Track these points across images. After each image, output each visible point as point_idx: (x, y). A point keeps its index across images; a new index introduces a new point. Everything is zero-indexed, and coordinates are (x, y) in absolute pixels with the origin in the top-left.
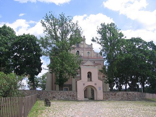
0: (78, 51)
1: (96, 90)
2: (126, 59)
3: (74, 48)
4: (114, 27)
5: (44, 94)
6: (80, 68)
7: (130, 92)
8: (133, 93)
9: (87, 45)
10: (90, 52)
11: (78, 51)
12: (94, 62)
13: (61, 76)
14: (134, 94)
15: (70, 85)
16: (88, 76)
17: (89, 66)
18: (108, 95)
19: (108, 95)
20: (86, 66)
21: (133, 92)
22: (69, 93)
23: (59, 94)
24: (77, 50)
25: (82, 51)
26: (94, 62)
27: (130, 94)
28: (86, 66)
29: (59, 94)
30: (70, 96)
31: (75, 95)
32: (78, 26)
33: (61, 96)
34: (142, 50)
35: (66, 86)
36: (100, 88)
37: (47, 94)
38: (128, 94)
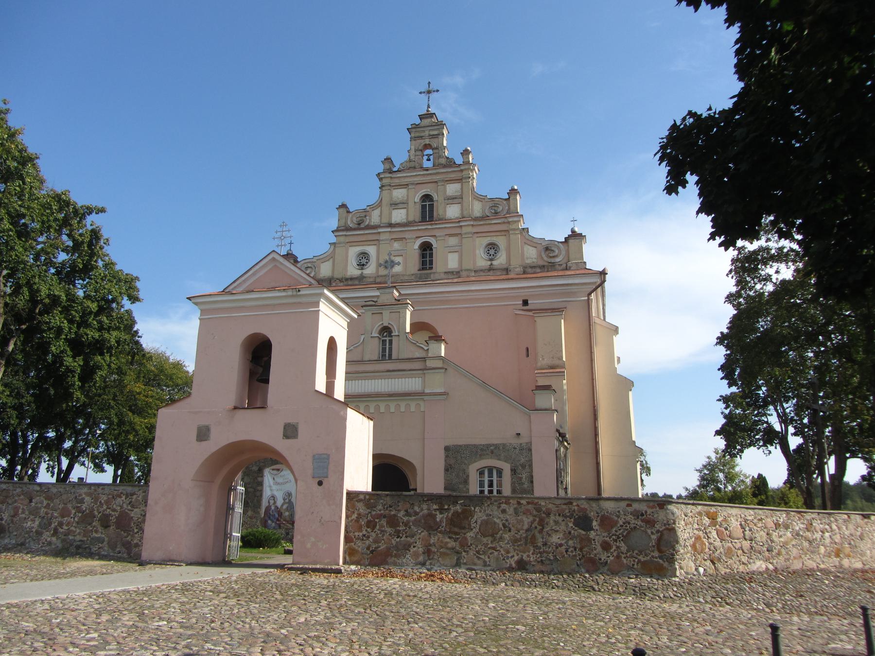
10: (501, 241)
11: (426, 248)
12: (525, 303)
19: (393, 522)
24: (418, 242)
25: (453, 241)
26: (525, 303)
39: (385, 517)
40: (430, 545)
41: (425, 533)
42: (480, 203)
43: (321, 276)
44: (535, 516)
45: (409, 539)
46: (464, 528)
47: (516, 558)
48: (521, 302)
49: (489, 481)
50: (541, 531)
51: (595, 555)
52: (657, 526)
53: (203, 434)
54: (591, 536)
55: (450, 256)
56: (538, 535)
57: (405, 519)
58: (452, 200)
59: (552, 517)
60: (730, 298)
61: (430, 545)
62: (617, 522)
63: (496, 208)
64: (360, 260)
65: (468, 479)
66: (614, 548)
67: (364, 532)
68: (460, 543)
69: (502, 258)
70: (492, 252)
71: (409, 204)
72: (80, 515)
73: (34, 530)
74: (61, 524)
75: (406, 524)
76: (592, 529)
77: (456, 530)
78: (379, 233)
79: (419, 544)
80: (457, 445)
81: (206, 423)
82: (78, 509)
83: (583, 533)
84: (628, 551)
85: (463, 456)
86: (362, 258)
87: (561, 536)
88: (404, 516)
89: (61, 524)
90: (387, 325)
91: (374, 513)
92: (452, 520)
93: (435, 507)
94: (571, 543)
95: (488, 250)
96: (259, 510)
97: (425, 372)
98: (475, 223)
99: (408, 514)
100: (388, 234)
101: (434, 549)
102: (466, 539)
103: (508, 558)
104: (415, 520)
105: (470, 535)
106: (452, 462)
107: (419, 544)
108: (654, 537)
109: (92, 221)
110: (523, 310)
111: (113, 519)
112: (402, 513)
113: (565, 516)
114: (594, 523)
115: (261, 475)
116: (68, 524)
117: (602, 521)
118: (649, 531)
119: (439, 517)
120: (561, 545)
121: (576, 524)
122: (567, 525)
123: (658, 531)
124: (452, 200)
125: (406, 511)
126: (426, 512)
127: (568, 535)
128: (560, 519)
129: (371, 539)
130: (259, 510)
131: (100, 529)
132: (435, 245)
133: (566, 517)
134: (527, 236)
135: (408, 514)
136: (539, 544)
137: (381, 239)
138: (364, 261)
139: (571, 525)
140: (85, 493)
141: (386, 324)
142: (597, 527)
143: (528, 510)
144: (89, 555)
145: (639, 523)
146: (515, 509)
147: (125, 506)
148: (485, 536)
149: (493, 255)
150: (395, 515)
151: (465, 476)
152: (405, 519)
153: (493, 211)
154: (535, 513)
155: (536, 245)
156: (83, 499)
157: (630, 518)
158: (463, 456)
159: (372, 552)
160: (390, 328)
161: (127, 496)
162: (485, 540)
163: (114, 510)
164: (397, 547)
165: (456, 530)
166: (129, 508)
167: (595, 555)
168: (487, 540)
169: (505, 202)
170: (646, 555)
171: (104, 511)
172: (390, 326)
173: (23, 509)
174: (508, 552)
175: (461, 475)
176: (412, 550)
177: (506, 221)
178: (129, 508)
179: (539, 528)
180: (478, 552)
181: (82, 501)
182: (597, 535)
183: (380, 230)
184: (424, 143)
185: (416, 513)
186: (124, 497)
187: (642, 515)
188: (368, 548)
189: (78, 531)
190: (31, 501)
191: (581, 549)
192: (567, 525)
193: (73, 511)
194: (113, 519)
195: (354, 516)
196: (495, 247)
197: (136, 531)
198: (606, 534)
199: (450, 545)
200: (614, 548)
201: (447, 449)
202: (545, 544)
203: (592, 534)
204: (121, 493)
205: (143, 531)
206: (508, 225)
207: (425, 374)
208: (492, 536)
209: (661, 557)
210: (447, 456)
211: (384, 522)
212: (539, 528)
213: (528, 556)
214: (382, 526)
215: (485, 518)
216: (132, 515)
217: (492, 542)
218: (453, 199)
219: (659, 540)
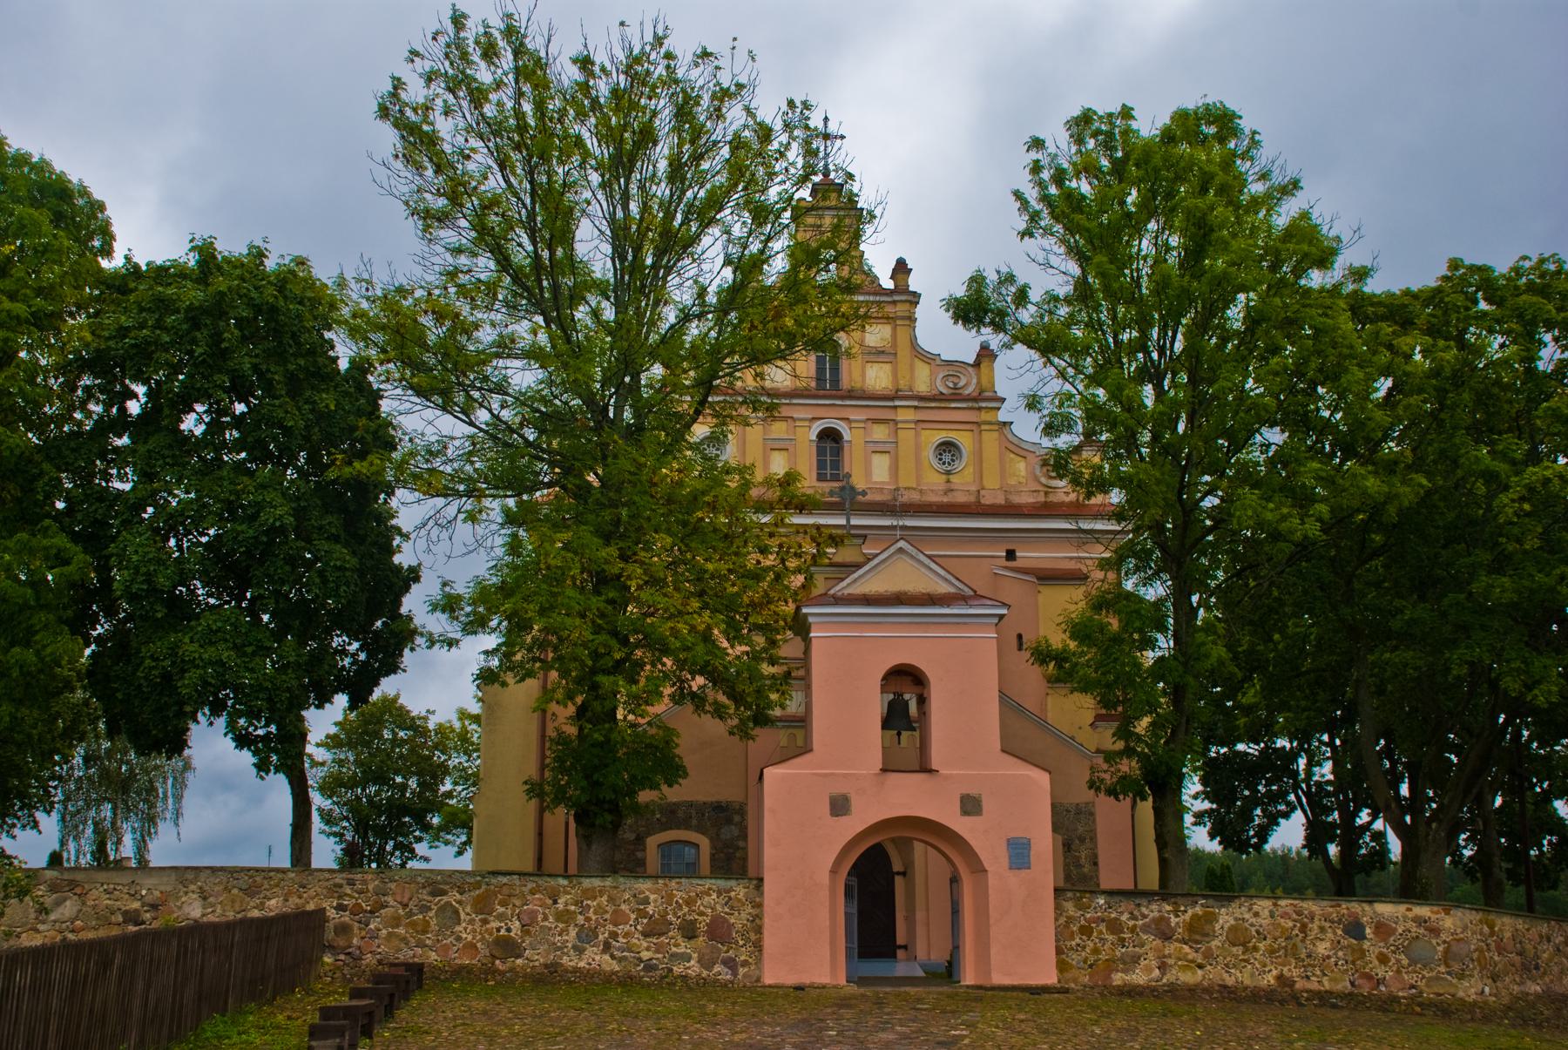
0: (830, 437)
1: (978, 869)
2: (1338, 523)
3: (768, 404)
4: (1234, 154)
5: (393, 908)
6: (801, 627)
7: (1385, 909)
8: (1420, 921)
9: (929, 358)
10: (964, 440)
11: (830, 437)
12: (1011, 555)
13: (595, 713)
14: (1435, 931)
15: (719, 808)
16: (896, 718)
17: (899, 599)
18: (1115, 927)
19: (1115, 927)
20: (867, 600)
21: (1423, 911)
22: (669, 898)
23: (560, 916)
24: (817, 427)
25: (880, 433)
26: (1011, 555)
27: (1383, 929)
28: (867, 600)
29: (560, 916)
30: (689, 932)
31: (739, 920)
32: (1052, 149)
33: (587, 936)
34: (96, 570)
35: (673, 816)
36: (1019, 853)
37: (425, 909)
38: (1355, 929)
39: (1103, 921)
40: (1165, 957)
41: (1158, 942)
42: (927, 366)
44: (1295, 921)
45: (1137, 949)
46: (1207, 935)
47: (1275, 972)
48: (1018, 554)
50: (1303, 941)
51: (1371, 969)
52: (1443, 936)
53: (839, 806)
54: (1365, 947)
55: (876, 459)
56: (1300, 945)
57: (1131, 923)
58: (877, 354)
59: (1317, 922)
61: (1165, 957)
62: (1396, 929)
63: (956, 380)
66: (1393, 961)
67: (1078, 940)
68: (1203, 953)
69: (966, 472)
70: (947, 457)
72: (645, 921)
73: (570, 945)
74: (614, 935)
75: (1133, 930)
76: (1364, 938)
77: (1198, 937)
78: (895, 407)
79: (1150, 955)
81: (844, 791)
82: (642, 914)
83: (1354, 942)
84: (1409, 965)
87: (1328, 945)
88: (1128, 919)
89: (614, 935)
91: (1088, 916)
92: (1190, 924)
93: (1169, 908)
94: (1340, 954)
98: (922, 404)
99: (1133, 917)
100: (912, 410)
101: (1171, 961)
102: (1210, 948)
103: (1264, 972)
104: (1144, 925)
105: (1215, 943)
107: (1150, 955)
108: (1440, 948)
109: (1060, 141)
110: (1006, 568)
111: (703, 927)
112: (1124, 917)
113: (1332, 922)
114: (1368, 931)
116: (626, 935)
117: (1376, 927)
118: (1434, 942)
119: (1174, 920)
120: (1329, 957)
121: (1347, 931)
122: (1335, 933)
123: (1445, 942)
124: (877, 354)
125: (1131, 913)
126: (1156, 914)
127: (1336, 944)
128: (1327, 925)
129: (1088, 950)
131: (680, 940)
132: (847, 436)
133: (1332, 922)
134: (1010, 437)
135: (1133, 917)
136: (1303, 956)
137: (899, 418)
139: (1339, 932)
140: (648, 890)
142: (1371, 936)
143: (1286, 913)
145: (1422, 931)
146: (1271, 912)
147: (719, 908)
148: (1234, 945)
150: (1116, 919)
152: (1131, 923)
153: (951, 385)
154: (1295, 916)
156: (647, 898)
157: (1410, 924)
159: (1091, 966)
161: (719, 893)
162: (1234, 949)
163: (702, 914)
164: (1122, 960)
165: (1198, 937)
166: (727, 910)
167: (1371, 969)
168: (1237, 950)
169: (970, 369)
170: (1431, 970)
171: (684, 915)
173: (544, 913)
174: (1265, 966)
176: (1143, 963)
177: (976, 405)
178: (727, 910)
179: (1301, 935)
180: (1226, 965)
181: (646, 901)
182: (1372, 946)
183: (897, 403)
185: (1145, 916)
186: (714, 896)
187: (1425, 922)
188: (1085, 961)
189: (645, 944)
190: (555, 902)
191: (1353, 963)
192: (1335, 933)
193: (633, 916)
194: (703, 927)
195: (1062, 920)
196: (957, 454)
197: (741, 943)
198: (1382, 944)
199: (1190, 957)
200: (1393, 961)
202: (1309, 956)
203: (1366, 945)
204: (710, 889)
205: (761, 950)
206: (977, 412)
208: (1244, 944)
209: (1449, 973)
211: (1103, 927)
212: (1301, 935)
213: (1290, 970)
214: (1101, 932)
215: (1232, 922)
216: (732, 921)
217: (1243, 953)
219: (1446, 952)
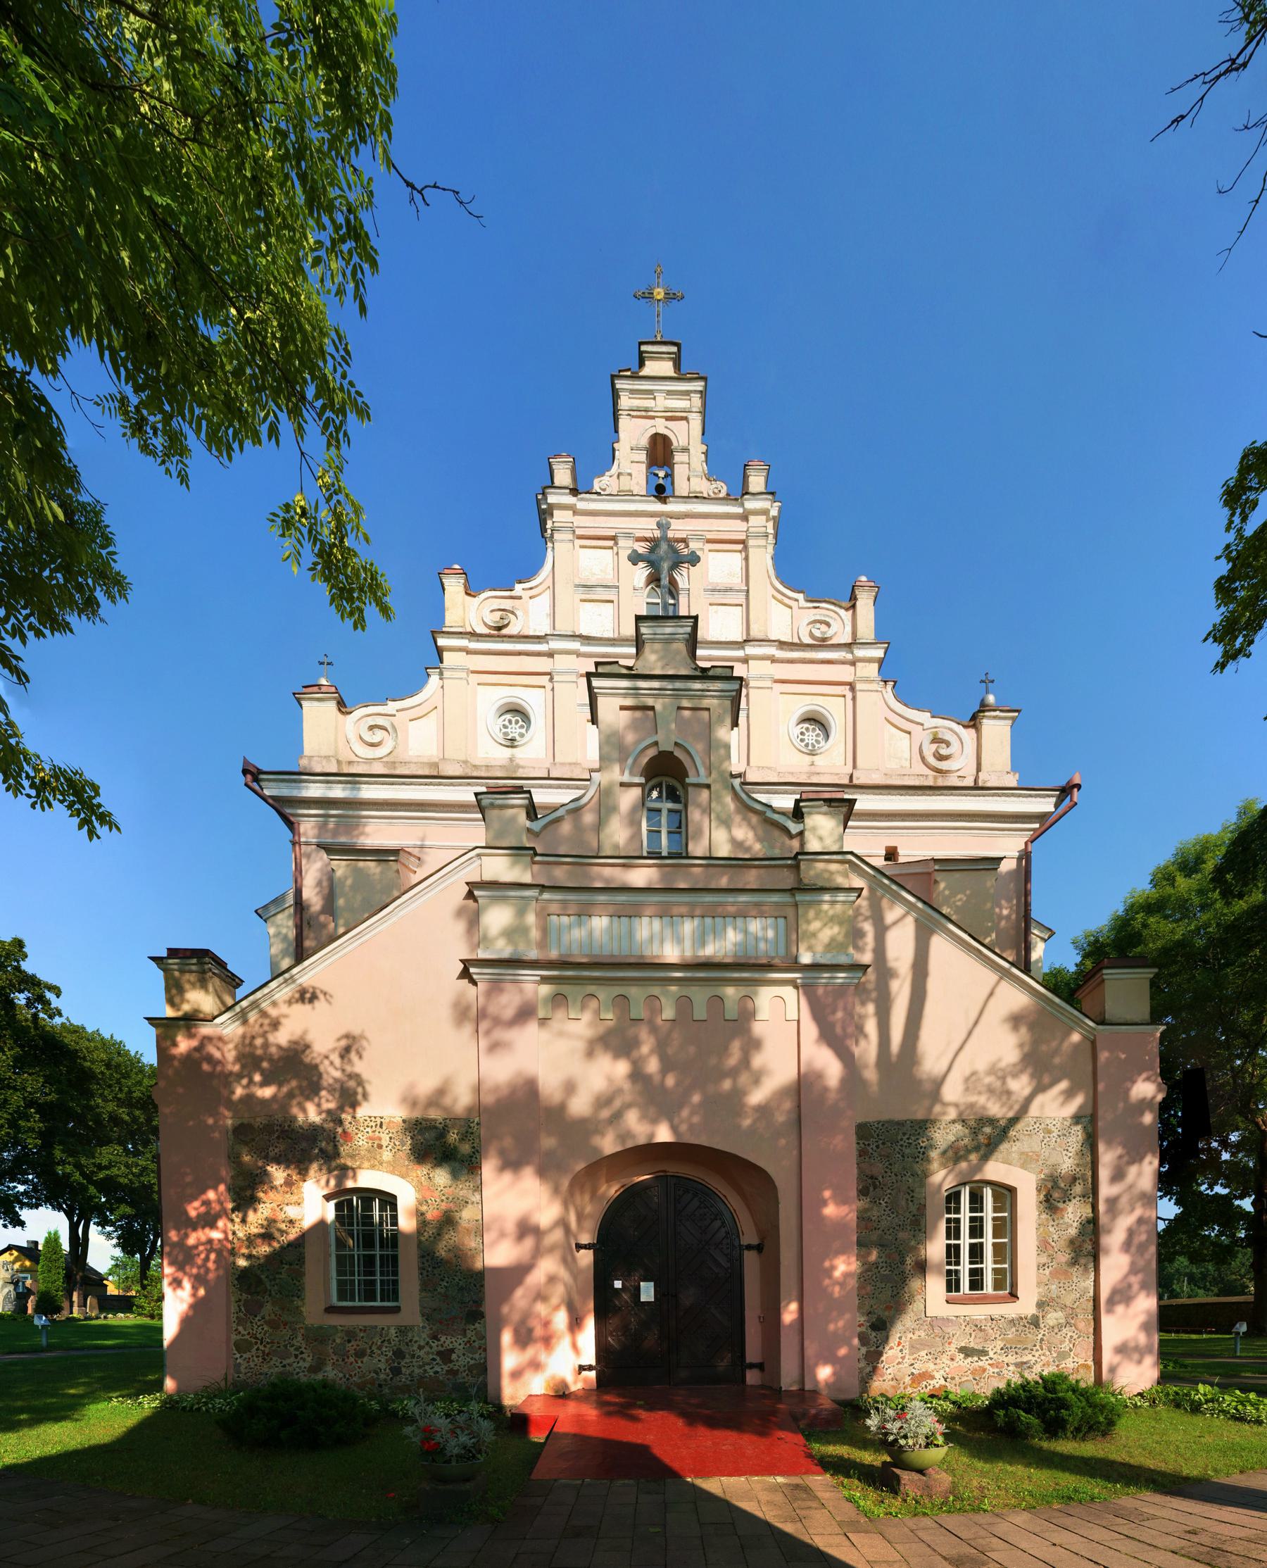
43: (411, 753)
48: (884, 853)
49: (972, 1219)
60: (1077, 965)
64: (505, 727)
65: (923, 1215)
71: (692, 451)
80: (890, 1122)
85: (907, 1151)
86: (510, 722)
90: (670, 749)
95: (802, 733)
96: (297, 1302)
97: (799, 897)
106: (878, 1168)
115: (294, 1198)
130: (297, 1302)
138: (514, 731)
141: (666, 746)
144: (752, 1216)
149: (813, 746)
151: (913, 1208)
155: (908, 726)
158: (907, 1151)
160: (679, 762)
172: (678, 753)
175: (903, 1203)
184: (653, 431)
190: (349, 1341)
201: (863, 1131)
207: (796, 905)
210: (862, 1153)
218: (726, 590)
